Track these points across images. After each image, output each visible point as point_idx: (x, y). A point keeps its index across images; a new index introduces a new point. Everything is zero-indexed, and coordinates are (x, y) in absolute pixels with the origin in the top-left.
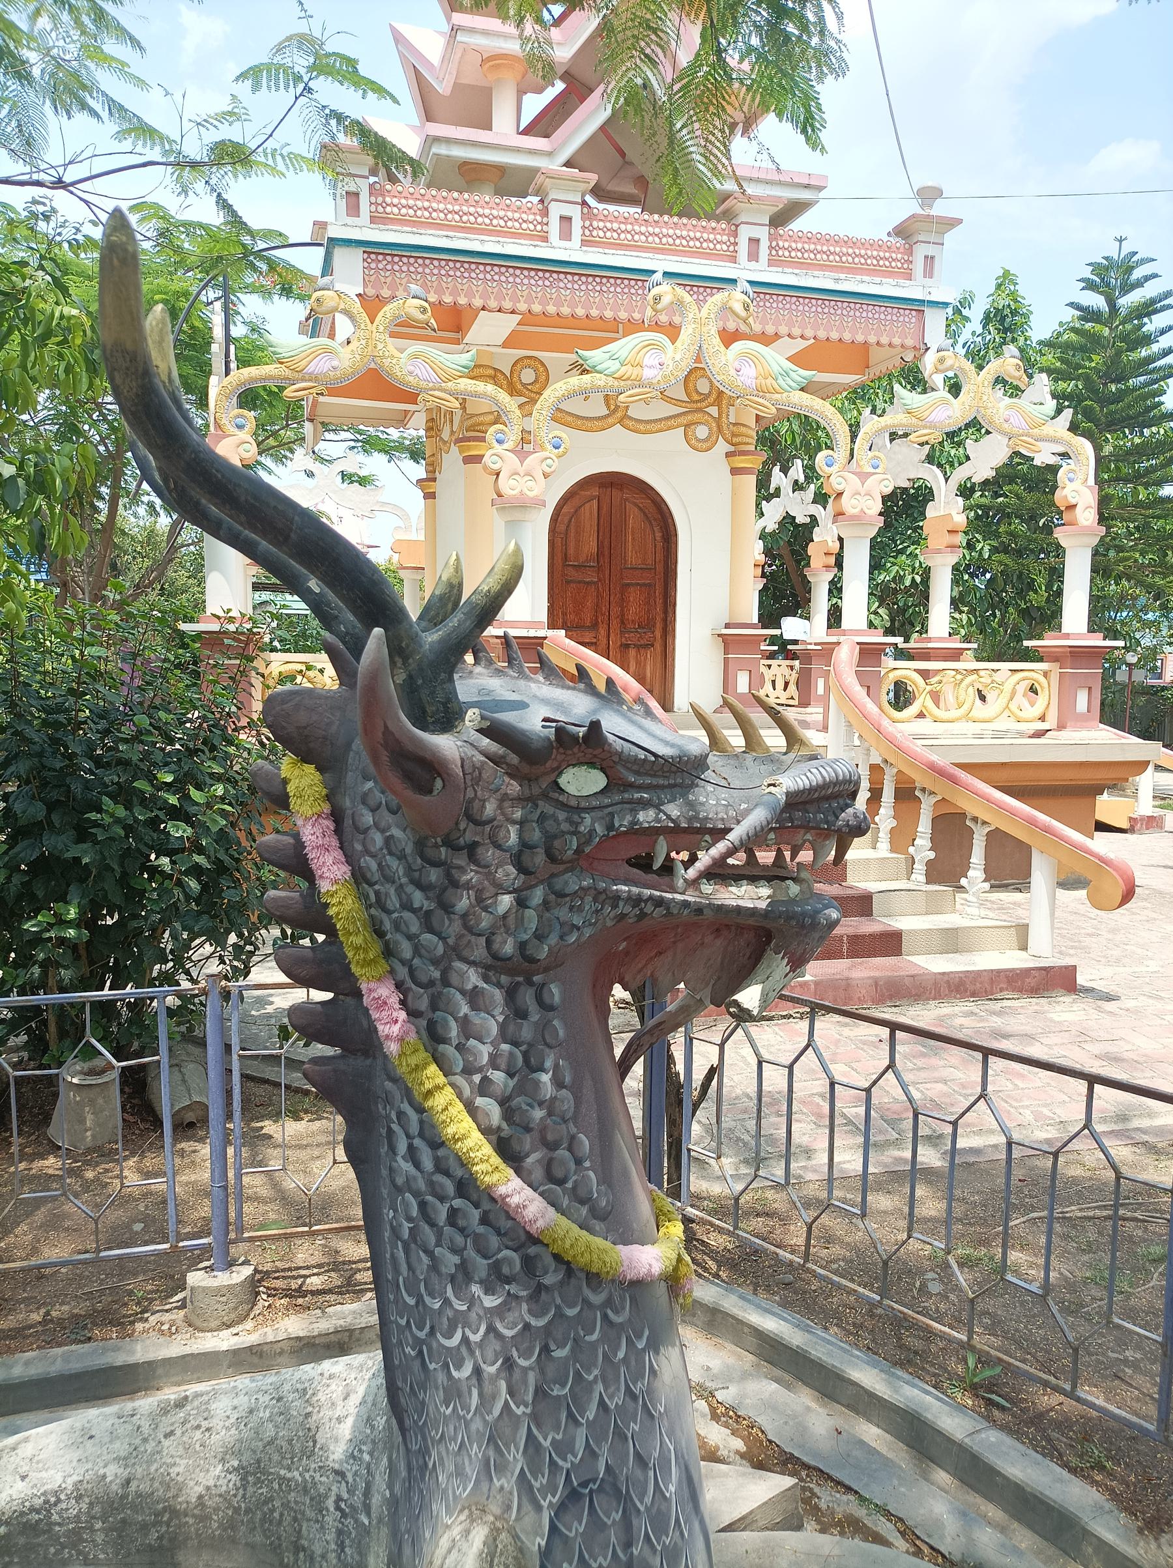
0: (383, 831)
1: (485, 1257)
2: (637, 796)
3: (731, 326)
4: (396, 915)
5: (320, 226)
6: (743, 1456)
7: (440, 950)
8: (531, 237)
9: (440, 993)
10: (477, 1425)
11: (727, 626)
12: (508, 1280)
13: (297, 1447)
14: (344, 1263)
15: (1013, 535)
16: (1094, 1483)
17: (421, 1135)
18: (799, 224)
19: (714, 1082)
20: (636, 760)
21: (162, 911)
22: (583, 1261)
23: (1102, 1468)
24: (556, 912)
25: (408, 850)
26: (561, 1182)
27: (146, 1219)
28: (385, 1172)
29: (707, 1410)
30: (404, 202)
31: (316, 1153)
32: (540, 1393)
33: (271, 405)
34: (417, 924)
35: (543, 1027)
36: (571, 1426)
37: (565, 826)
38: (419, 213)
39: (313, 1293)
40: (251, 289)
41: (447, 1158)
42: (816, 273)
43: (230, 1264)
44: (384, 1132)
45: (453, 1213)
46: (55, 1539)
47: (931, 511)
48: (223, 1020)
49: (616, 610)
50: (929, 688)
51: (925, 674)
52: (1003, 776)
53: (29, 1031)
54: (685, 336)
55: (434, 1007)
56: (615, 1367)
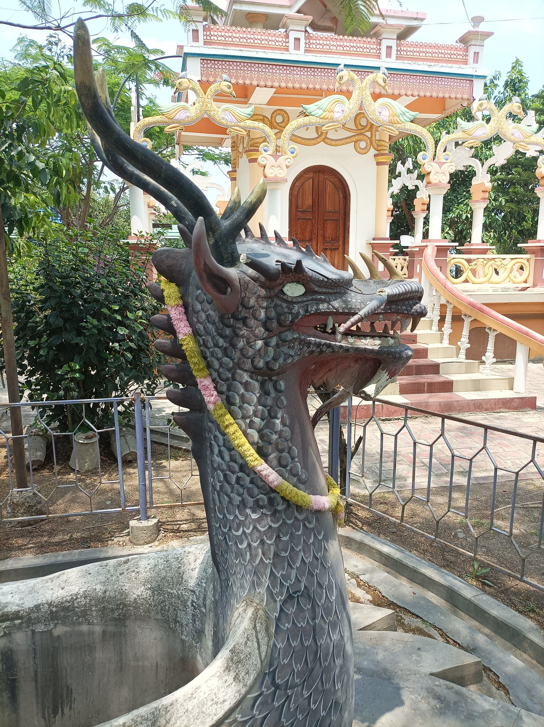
0: (205, 312)
1: (252, 497)
2: (319, 297)
3: (377, 91)
4: (211, 349)
5: (180, 47)
6: (371, 602)
7: (231, 364)
8: (280, 49)
9: (231, 384)
10: (249, 567)
11: (374, 239)
12: (262, 507)
13: (175, 580)
14: (197, 519)
15: (516, 193)
16: (530, 617)
17: (224, 445)
18: (412, 39)
19: (362, 444)
20: (319, 280)
21: (115, 367)
22: (294, 500)
23: (533, 611)
24: (282, 349)
25: (216, 320)
26: (285, 467)
27: (111, 499)
28: (209, 462)
29: (356, 583)
30: (219, 34)
31: (185, 474)
32: (276, 555)
33: (159, 138)
34: (221, 353)
35: (277, 399)
36: (289, 569)
37: (286, 310)
38: (227, 39)
39: (183, 531)
40: (150, 82)
41: (235, 455)
42: (419, 63)
43: (148, 518)
44: (208, 445)
45: (238, 479)
46: (76, 614)
47: (474, 182)
48: (142, 417)
49: (320, 232)
50: (470, 267)
51: (469, 261)
52: (506, 309)
53: (59, 420)
54: (354, 96)
55: (229, 389)
56: (309, 546)
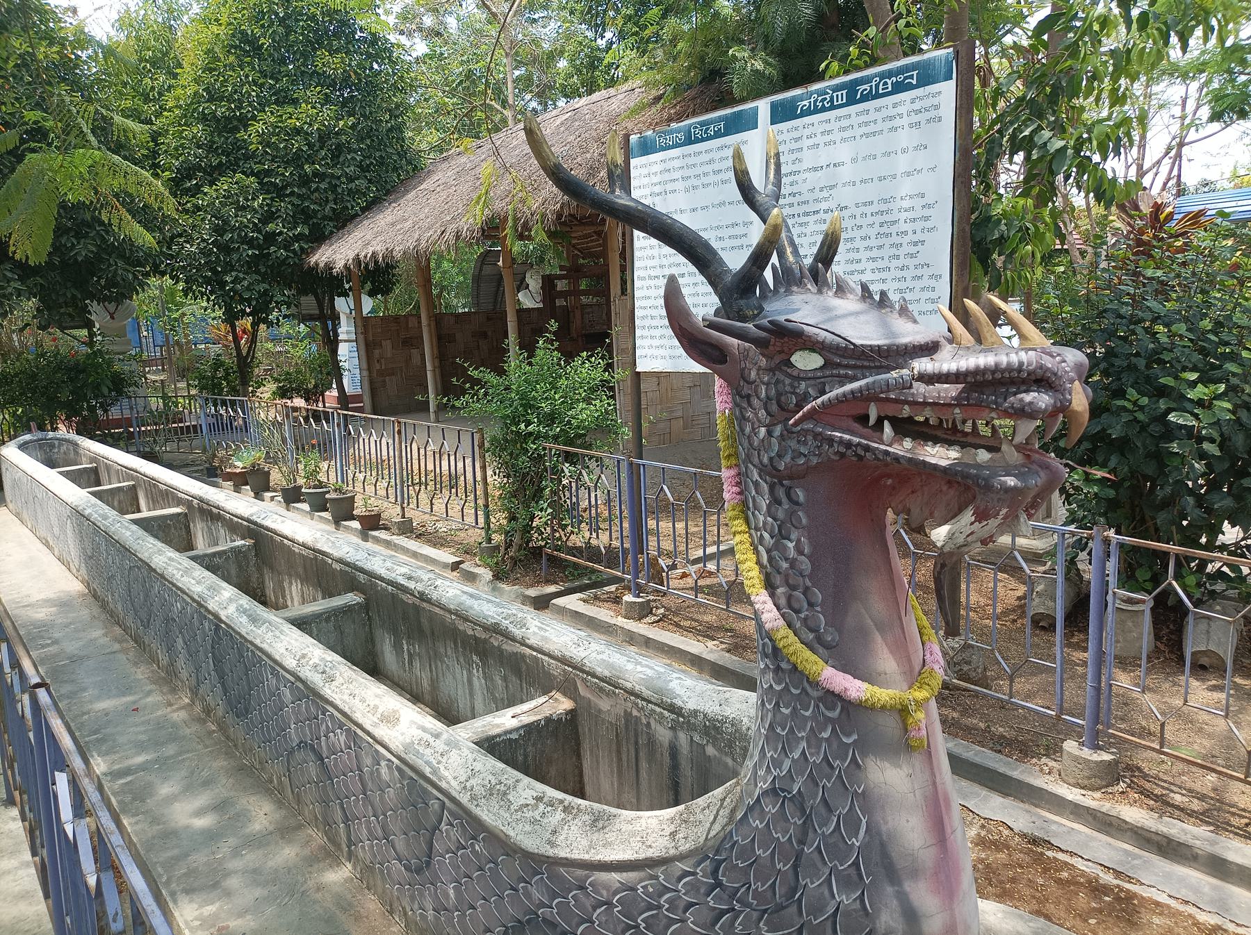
20: (838, 347)
26: (797, 612)
35: (791, 514)
36: (783, 755)
37: (788, 388)
